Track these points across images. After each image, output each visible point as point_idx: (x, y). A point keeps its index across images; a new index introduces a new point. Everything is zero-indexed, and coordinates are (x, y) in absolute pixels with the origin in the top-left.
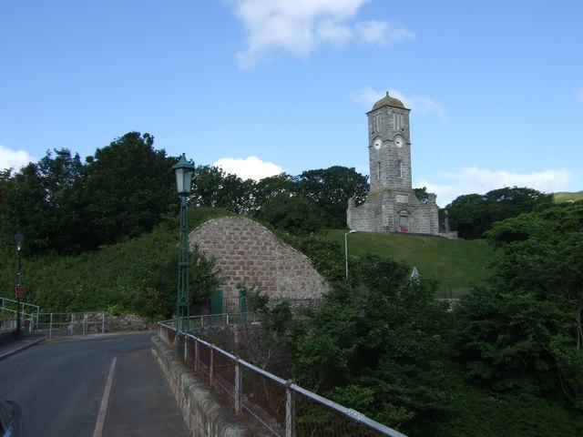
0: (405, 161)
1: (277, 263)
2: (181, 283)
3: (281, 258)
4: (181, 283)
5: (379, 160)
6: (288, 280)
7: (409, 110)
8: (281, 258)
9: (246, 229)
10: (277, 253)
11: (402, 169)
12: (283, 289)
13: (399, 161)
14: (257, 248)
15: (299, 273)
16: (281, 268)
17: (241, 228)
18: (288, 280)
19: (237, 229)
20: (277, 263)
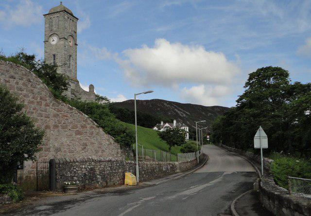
0: (74, 56)
1: (52, 123)
2: (201, 133)
3: (56, 116)
4: (201, 133)
5: (54, 53)
6: (64, 140)
7: (78, 19)
8: (56, 116)
9: (22, 79)
10: (51, 111)
11: (72, 62)
12: (58, 150)
13: (70, 56)
14: (32, 102)
15: (78, 133)
16: (56, 126)
17: (16, 76)
18: (64, 140)
19: (12, 77)
20: (52, 123)
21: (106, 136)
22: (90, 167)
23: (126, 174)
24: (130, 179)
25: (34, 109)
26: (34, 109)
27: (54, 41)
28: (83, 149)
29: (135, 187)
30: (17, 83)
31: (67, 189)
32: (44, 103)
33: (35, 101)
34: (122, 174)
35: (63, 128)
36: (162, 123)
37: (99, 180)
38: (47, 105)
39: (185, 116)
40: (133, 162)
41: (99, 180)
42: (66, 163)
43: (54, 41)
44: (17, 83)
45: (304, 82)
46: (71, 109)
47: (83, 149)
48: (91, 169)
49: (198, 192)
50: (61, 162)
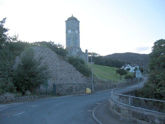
9: (46, 53)
12: (61, 79)
15: (69, 73)
16: (60, 70)
18: (64, 75)
21: (80, 74)
22: (70, 86)
23: (87, 89)
24: (89, 90)
25: (51, 64)
26: (51, 64)
27: (70, 31)
28: (71, 79)
29: (89, 94)
30: (44, 54)
31: (59, 95)
32: (55, 61)
33: (52, 61)
34: (85, 89)
35: (63, 70)
36: (126, 64)
37: (74, 91)
38: (56, 62)
39: (142, 60)
40: (91, 84)
41: (74, 91)
42: (59, 85)
43: (70, 31)
44: (44, 54)
45: (164, 39)
46: (66, 63)
47: (71, 79)
48: (71, 87)
49: (154, 101)
50: (58, 84)
